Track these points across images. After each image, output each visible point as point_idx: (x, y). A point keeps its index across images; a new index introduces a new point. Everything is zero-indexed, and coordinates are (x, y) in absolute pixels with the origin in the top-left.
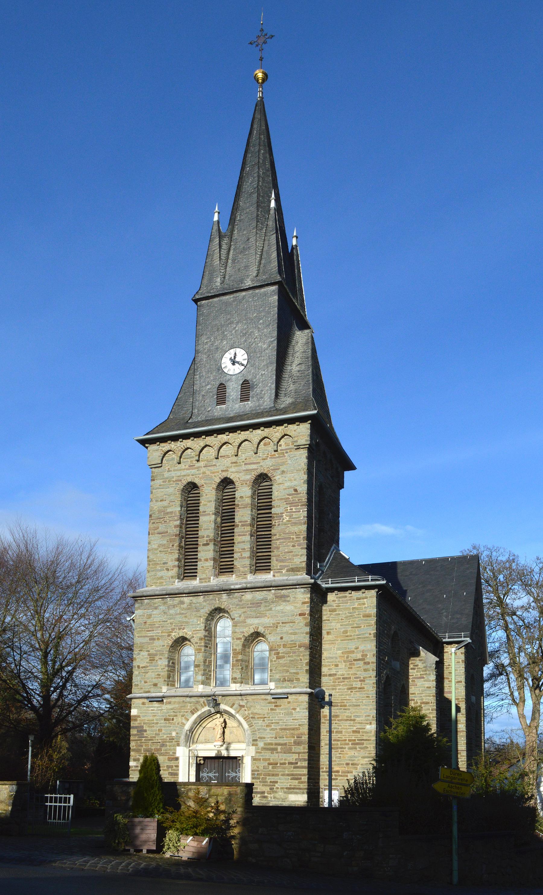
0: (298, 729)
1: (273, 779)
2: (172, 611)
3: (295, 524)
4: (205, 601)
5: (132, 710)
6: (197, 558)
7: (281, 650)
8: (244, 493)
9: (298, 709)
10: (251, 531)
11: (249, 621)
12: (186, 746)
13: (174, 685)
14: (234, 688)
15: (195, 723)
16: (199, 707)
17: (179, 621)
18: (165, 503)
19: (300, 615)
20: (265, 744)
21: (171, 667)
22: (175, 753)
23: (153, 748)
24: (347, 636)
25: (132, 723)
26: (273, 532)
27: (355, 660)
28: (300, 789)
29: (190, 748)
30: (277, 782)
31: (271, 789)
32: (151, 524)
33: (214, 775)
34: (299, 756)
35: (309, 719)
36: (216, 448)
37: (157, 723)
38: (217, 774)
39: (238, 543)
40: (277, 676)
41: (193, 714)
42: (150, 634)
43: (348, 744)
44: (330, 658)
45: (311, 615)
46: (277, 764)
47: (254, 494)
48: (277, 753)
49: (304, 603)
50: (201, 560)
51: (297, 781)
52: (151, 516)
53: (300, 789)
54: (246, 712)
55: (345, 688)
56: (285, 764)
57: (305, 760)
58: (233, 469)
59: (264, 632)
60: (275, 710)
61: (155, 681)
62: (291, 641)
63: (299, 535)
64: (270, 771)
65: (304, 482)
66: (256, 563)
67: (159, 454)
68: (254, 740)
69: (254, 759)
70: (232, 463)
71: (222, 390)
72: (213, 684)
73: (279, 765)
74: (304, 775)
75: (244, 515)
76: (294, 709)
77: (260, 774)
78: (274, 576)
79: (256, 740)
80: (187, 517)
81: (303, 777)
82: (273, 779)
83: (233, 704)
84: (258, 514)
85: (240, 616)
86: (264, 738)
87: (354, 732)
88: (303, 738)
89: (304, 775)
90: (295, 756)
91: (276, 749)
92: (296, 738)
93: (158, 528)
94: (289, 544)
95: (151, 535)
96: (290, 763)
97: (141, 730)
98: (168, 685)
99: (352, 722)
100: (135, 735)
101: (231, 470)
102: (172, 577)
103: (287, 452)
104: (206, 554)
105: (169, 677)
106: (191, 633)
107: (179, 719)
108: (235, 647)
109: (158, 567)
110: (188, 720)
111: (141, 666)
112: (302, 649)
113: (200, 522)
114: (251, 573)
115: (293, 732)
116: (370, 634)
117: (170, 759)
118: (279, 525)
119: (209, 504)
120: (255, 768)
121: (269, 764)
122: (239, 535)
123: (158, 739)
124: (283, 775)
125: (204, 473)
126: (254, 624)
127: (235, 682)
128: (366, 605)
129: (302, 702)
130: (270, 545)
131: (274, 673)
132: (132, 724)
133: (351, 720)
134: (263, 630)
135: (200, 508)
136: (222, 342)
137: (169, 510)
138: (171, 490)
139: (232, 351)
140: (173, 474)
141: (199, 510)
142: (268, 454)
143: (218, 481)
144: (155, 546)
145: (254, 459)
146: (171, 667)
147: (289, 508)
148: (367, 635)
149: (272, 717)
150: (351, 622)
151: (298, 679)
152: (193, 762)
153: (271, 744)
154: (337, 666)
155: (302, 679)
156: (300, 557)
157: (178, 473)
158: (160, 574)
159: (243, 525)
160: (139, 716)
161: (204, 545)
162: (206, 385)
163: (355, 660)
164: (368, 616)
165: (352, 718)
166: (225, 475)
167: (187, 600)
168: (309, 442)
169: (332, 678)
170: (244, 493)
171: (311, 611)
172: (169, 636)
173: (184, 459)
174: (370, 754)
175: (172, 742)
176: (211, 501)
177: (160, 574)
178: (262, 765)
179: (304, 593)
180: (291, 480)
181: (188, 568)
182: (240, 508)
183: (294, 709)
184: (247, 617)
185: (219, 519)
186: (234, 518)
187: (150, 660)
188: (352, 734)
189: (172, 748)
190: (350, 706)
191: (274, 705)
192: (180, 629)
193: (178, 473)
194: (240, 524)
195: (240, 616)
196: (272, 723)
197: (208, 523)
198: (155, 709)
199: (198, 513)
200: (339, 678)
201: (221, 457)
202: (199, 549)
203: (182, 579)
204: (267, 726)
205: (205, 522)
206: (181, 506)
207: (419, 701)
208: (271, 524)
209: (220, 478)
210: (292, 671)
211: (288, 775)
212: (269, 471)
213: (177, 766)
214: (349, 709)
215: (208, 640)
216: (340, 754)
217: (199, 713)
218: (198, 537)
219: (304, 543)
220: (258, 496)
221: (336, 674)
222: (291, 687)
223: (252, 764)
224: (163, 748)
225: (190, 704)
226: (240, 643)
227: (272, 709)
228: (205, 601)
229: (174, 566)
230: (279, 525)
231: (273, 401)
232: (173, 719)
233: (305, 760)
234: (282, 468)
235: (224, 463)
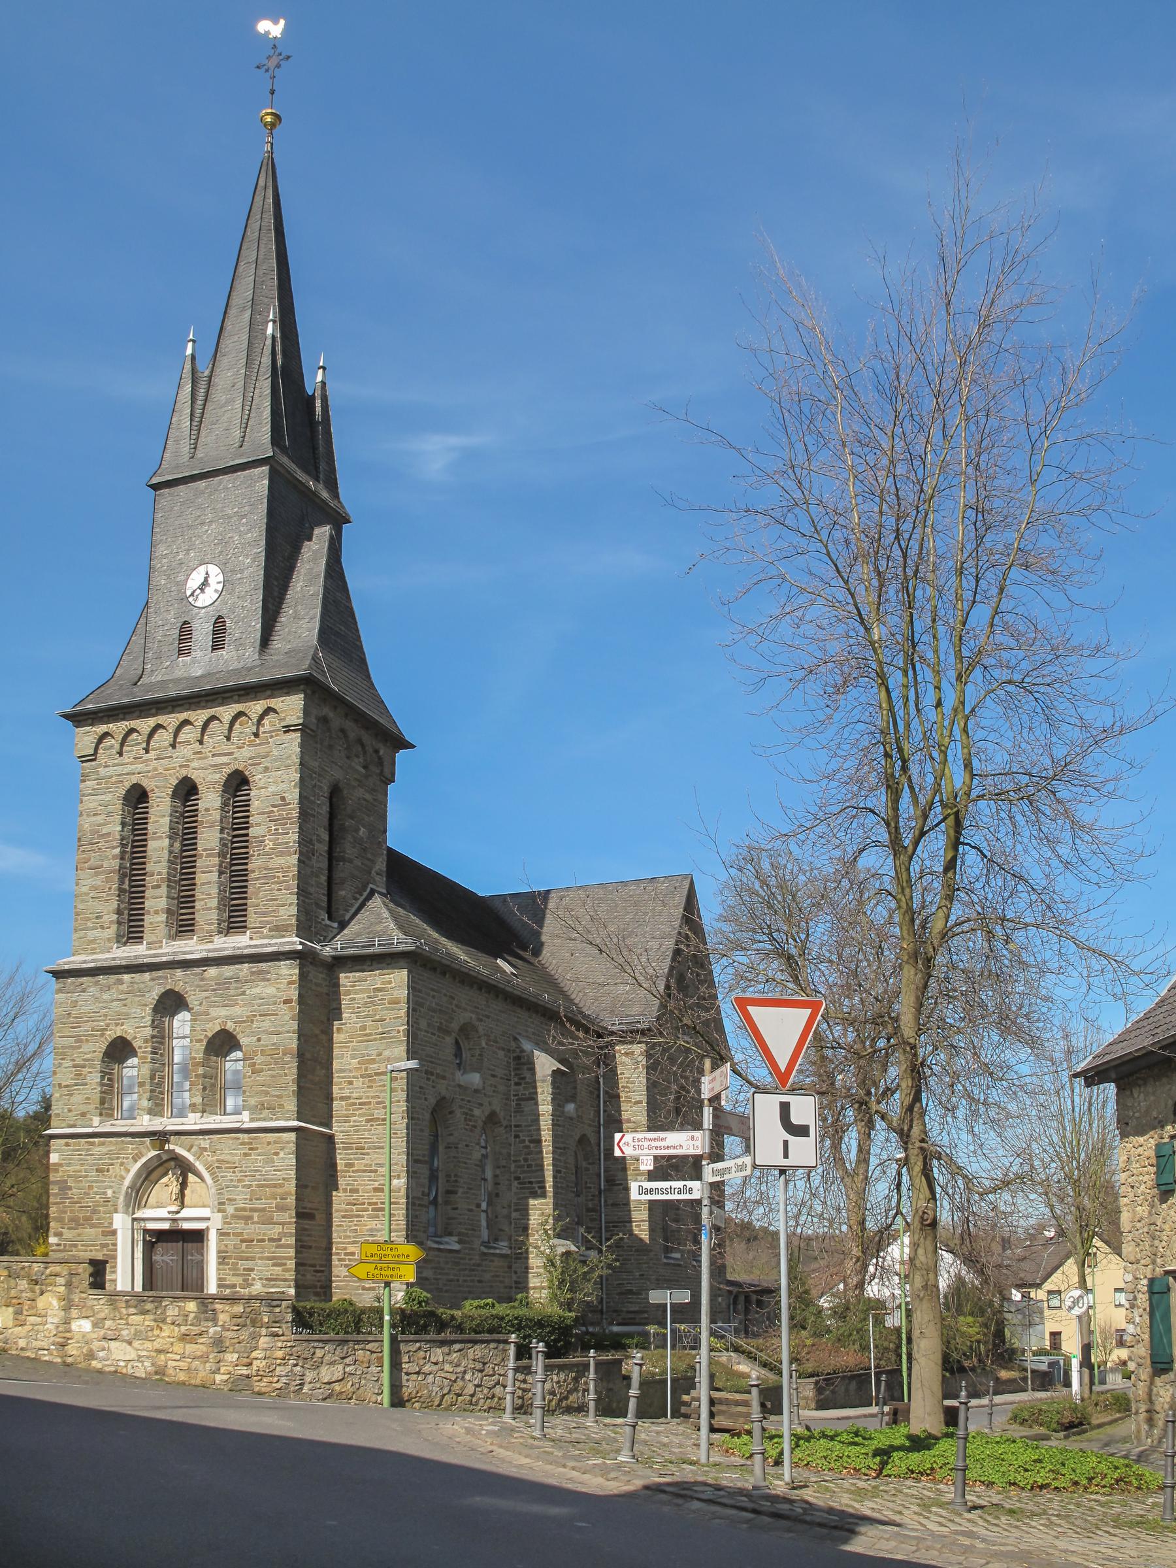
0: (281, 1186)
1: (249, 1264)
2: (106, 996)
3: (282, 854)
4: (152, 980)
5: (51, 1155)
7: (259, 1059)
8: (210, 802)
9: (282, 1155)
10: (220, 866)
11: (214, 1012)
12: (126, 1212)
13: (112, 1115)
14: (193, 1121)
15: (138, 1174)
16: (144, 1151)
18: (100, 819)
19: (286, 1002)
20: (236, 1210)
22: (111, 1224)
24: (365, 1035)
25: (51, 1175)
27: (377, 1074)
28: (285, 1280)
30: (252, 1270)
31: (244, 1280)
36: (171, 729)
37: (86, 1176)
39: (202, 884)
40: (253, 1101)
42: (76, 1032)
44: (343, 1071)
45: (300, 1003)
47: (225, 804)
49: (290, 983)
51: (280, 1268)
53: (285, 1280)
54: (210, 1159)
56: (263, 1240)
57: (290, 1235)
61: (83, 1108)
66: (230, 917)
68: (220, 1204)
69: (221, 1233)
74: (290, 1258)
76: (277, 1154)
78: (251, 938)
79: (223, 1203)
82: (249, 1264)
83: (192, 1147)
84: (235, 836)
85: (201, 1004)
89: (290, 1258)
91: (251, 1218)
97: (64, 1187)
98: (101, 1115)
100: (56, 1195)
101: (193, 765)
102: (109, 939)
103: (272, 737)
104: (157, 901)
105: (102, 1102)
107: (116, 1170)
109: (90, 924)
111: (64, 1084)
113: (149, 848)
114: (220, 932)
115: (273, 1189)
117: (105, 1234)
120: (223, 1248)
121: (242, 1241)
122: (204, 872)
125: (155, 769)
126: (221, 1017)
127: (193, 1112)
129: (288, 1142)
132: (53, 1177)
133: (371, 1171)
134: (233, 1026)
135: (149, 827)
137: (105, 830)
138: (108, 797)
140: (111, 771)
141: (146, 829)
144: (84, 889)
145: (225, 748)
152: (139, 1237)
153: (244, 1209)
154: (351, 1083)
155: (287, 1107)
156: (289, 911)
157: (119, 769)
158: (91, 935)
160: (61, 1165)
161: (154, 887)
162: (164, 623)
163: (377, 1074)
164: (396, 1002)
166: (184, 772)
167: (126, 977)
169: (344, 1103)
171: (300, 995)
177: (91, 935)
178: (231, 1242)
181: (131, 927)
183: (277, 1154)
185: (177, 845)
186: (196, 844)
190: (369, 1148)
193: (119, 769)
195: (201, 1004)
197: (159, 848)
199: (145, 834)
200: (354, 1104)
202: (147, 894)
203: (125, 944)
205: (155, 849)
206: (123, 824)
211: (269, 1258)
213: (115, 1245)
214: (368, 1154)
217: (144, 1160)
218: (144, 874)
220: (235, 807)
221: (349, 1097)
223: (219, 1241)
224: (95, 1216)
225: (131, 1145)
226: (201, 1047)
228: (152, 980)
229: (111, 922)
232: (108, 1170)
233: (290, 1235)
234: (265, 763)
235: (184, 751)
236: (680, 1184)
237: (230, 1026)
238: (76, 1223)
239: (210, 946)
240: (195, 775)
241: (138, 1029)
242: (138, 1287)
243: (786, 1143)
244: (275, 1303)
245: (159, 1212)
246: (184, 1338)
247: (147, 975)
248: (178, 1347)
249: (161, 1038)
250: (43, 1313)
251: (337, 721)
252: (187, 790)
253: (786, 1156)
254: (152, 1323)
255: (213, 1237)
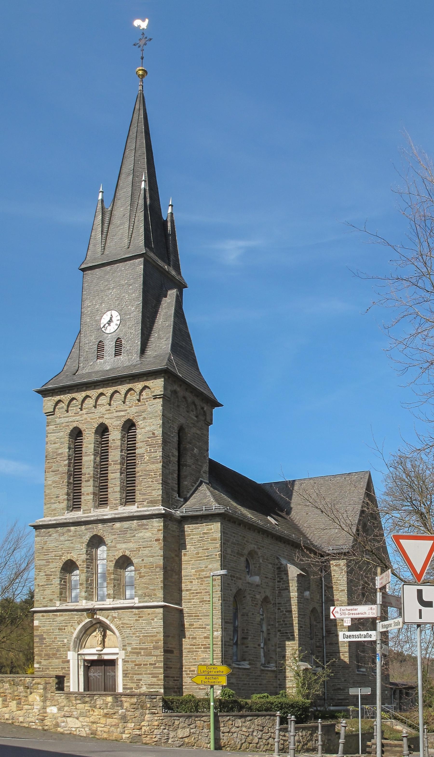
0: (156, 636)
1: (140, 677)
2: (62, 538)
3: (153, 463)
4: (86, 529)
5: (35, 622)
6: (81, 492)
7: (143, 570)
8: (115, 436)
9: (156, 620)
10: (121, 469)
11: (119, 546)
12: (74, 651)
13: (66, 601)
14: (109, 603)
15: (80, 631)
16: (83, 619)
17: (67, 546)
18: (57, 445)
20: (132, 649)
21: (63, 585)
22: (67, 657)
23: (51, 653)
26: (137, 470)
27: (205, 577)
29: (79, 653)
30: (141, 680)
31: (137, 685)
32: (47, 463)
33: (110, 674)
34: (157, 658)
35: (164, 627)
36: (94, 398)
37: (53, 632)
38: (108, 674)
39: (112, 479)
40: (140, 592)
41: (79, 624)
42: (46, 557)
43: (201, 648)
44: (187, 576)
46: (141, 665)
47: (123, 437)
48: (141, 656)
49: (159, 530)
50: (84, 494)
51: (156, 679)
52: (46, 457)
55: (198, 601)
56: (147, 665)
58: (107, 416)
59: (130, 555)
60: (139, 620)
61: (51, 597)
62: (150, 563)
63: (156, 472)
64: (136, 671)
65: (160, 426)
66: (127, 496)
67: (52, 403)
68: (124, 646)
69: (124, 661)
70: (106, 411)
71: (100, 347)
72: (95, 598)
73: (142, 666)
74: (161, 674)
75: (115, 455)
76: (153, 620)
77: (129, 673)
78: (138, 507)
79: (125, 646)
80: (75, 457)
81: (160, 676)
82: (140, 677)
83: (108, 616)
85: (112, 542)
86: (131, 644)
87: (205, 638)
88: (160, 644)
89: (161, 674)
90: (154, 658)
91: (140, 653)
92: (154, 644)
93: (52, 467)
94: (149, 480)
95: (47, 473)
96: (151, 664)
97: (42, 638)
98: (60, 600)
99: (204, 629)
100: (37, 642)
102: (63, 509)
103: (147, 401)
104: (88, 489)
105: (61, 594)
106: (76, 557)
108: (108, 569)
109: (53, 501)
110: (76, 629)
111: (40, 584)
112: (158, 570)
113: (83, 461)
114: (121, 504)
115: (151, 638)
116: (216, 555)
118: (141, 463)
119: (89, 446)
120: (125, 669)
121: (136, 665)
123: (54, 645)
124: (145, 674)
126: (123, 548)
127: (109, 598)
128: (213, 531)
129: (159, 614)
130: (135, 480)
131: (137, 590)
132: (35, 633)
133: (203, 628)
135: (83, 449)
136: (101, 305)
137: (60, 451)
138: (61, 434)
139: (109, 313)
142: (133, 403)
143: (96, 426)
144: (50, 483)
145: (122, 407)
146: (63, 585)
147: (149, 449)
148: (214, 556)
149: (137, 626)
150: (201, 545)
151: (155, 595)
152: (81, 663)
153: (136, 649)
157: (67, 419)
158: (54, 506)
159: (114, 464)
160: (40, 627)
162: (89, 342)
163: (205, 577)
164: (215, 539)
165: (204, 626)
166: (101, 421)
167: (72, 528)
168: (162, 393)
169: (188, 593)
170: (115, 436)
171: (164, 537)
172: (60, 559)
173: (71, 407)
174: (217, 656)
175: (64, 648)
176: (91, 444)
177: (54, 506)
178: (130, 666)
179: (159, 522)
180: (150, 425)
182: (112, 449)
183: (153, 620)
184: (117, 543)
185: (98, 459)
187: (47, 580)
188: (204, 640)
189: (65, 652)
191: (138, 616)
192: (68, 553)
193: (67, 419)
194: (113, 463)
195: (112, 542)
196: (137, 631)
197: (88, 461)
198: (51, 620)
200: (193, 593)
201: (99, 405)
202: (82, 485)
203: (71, 511)
204: (133, 634)
206: (69, 448)
207: (284, 610)
208: (135, 463)
209: (97, 423)
210: (151, 588)
211: (149, 674)
212: (134, 417)
213: (69, 668)
214: (201, 619)
215: (89, 562)
216: (195, 656)
217: (83, 623)
218: (81, 474)
219: (160, 478)
221: (191, 590)
222: (150, 601)
224: (58, 653)
225: (76, 616)
227: (136, 620)
229: (64, 500)
230: (141, 463)
231: (139, 355)
236: (365, 633)
237: (127, 553)
238: (48, 657)
239: (116, 512)
240: (107, 422)
241: (79, 555)
242: (82, 690)
243: (420, 611)
244: (153, 697)
245: (91, 651)
246: (106, 715)
247: (83, 527)
248: (103, 720)
249: (91, 560)
250: (32, 703)
251: (181, 392)
252: (103, 430)
253: (420, 617)
254: (89, 708)
255: (120, 663)
